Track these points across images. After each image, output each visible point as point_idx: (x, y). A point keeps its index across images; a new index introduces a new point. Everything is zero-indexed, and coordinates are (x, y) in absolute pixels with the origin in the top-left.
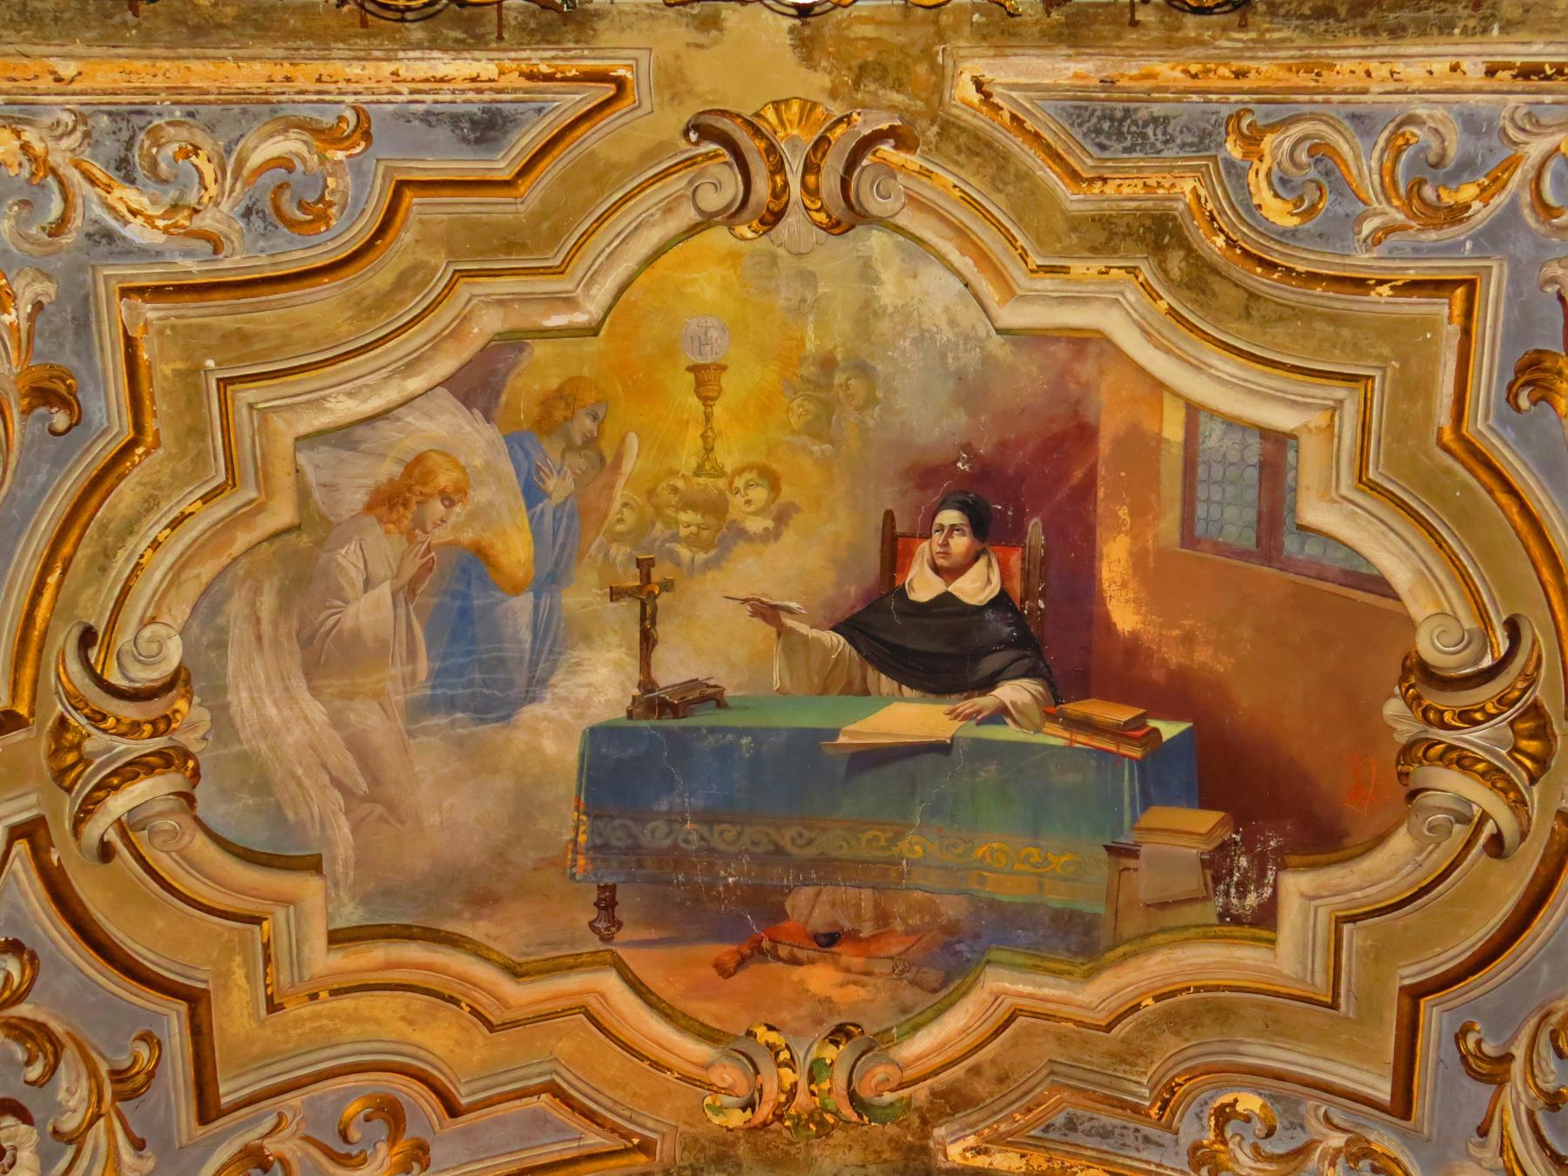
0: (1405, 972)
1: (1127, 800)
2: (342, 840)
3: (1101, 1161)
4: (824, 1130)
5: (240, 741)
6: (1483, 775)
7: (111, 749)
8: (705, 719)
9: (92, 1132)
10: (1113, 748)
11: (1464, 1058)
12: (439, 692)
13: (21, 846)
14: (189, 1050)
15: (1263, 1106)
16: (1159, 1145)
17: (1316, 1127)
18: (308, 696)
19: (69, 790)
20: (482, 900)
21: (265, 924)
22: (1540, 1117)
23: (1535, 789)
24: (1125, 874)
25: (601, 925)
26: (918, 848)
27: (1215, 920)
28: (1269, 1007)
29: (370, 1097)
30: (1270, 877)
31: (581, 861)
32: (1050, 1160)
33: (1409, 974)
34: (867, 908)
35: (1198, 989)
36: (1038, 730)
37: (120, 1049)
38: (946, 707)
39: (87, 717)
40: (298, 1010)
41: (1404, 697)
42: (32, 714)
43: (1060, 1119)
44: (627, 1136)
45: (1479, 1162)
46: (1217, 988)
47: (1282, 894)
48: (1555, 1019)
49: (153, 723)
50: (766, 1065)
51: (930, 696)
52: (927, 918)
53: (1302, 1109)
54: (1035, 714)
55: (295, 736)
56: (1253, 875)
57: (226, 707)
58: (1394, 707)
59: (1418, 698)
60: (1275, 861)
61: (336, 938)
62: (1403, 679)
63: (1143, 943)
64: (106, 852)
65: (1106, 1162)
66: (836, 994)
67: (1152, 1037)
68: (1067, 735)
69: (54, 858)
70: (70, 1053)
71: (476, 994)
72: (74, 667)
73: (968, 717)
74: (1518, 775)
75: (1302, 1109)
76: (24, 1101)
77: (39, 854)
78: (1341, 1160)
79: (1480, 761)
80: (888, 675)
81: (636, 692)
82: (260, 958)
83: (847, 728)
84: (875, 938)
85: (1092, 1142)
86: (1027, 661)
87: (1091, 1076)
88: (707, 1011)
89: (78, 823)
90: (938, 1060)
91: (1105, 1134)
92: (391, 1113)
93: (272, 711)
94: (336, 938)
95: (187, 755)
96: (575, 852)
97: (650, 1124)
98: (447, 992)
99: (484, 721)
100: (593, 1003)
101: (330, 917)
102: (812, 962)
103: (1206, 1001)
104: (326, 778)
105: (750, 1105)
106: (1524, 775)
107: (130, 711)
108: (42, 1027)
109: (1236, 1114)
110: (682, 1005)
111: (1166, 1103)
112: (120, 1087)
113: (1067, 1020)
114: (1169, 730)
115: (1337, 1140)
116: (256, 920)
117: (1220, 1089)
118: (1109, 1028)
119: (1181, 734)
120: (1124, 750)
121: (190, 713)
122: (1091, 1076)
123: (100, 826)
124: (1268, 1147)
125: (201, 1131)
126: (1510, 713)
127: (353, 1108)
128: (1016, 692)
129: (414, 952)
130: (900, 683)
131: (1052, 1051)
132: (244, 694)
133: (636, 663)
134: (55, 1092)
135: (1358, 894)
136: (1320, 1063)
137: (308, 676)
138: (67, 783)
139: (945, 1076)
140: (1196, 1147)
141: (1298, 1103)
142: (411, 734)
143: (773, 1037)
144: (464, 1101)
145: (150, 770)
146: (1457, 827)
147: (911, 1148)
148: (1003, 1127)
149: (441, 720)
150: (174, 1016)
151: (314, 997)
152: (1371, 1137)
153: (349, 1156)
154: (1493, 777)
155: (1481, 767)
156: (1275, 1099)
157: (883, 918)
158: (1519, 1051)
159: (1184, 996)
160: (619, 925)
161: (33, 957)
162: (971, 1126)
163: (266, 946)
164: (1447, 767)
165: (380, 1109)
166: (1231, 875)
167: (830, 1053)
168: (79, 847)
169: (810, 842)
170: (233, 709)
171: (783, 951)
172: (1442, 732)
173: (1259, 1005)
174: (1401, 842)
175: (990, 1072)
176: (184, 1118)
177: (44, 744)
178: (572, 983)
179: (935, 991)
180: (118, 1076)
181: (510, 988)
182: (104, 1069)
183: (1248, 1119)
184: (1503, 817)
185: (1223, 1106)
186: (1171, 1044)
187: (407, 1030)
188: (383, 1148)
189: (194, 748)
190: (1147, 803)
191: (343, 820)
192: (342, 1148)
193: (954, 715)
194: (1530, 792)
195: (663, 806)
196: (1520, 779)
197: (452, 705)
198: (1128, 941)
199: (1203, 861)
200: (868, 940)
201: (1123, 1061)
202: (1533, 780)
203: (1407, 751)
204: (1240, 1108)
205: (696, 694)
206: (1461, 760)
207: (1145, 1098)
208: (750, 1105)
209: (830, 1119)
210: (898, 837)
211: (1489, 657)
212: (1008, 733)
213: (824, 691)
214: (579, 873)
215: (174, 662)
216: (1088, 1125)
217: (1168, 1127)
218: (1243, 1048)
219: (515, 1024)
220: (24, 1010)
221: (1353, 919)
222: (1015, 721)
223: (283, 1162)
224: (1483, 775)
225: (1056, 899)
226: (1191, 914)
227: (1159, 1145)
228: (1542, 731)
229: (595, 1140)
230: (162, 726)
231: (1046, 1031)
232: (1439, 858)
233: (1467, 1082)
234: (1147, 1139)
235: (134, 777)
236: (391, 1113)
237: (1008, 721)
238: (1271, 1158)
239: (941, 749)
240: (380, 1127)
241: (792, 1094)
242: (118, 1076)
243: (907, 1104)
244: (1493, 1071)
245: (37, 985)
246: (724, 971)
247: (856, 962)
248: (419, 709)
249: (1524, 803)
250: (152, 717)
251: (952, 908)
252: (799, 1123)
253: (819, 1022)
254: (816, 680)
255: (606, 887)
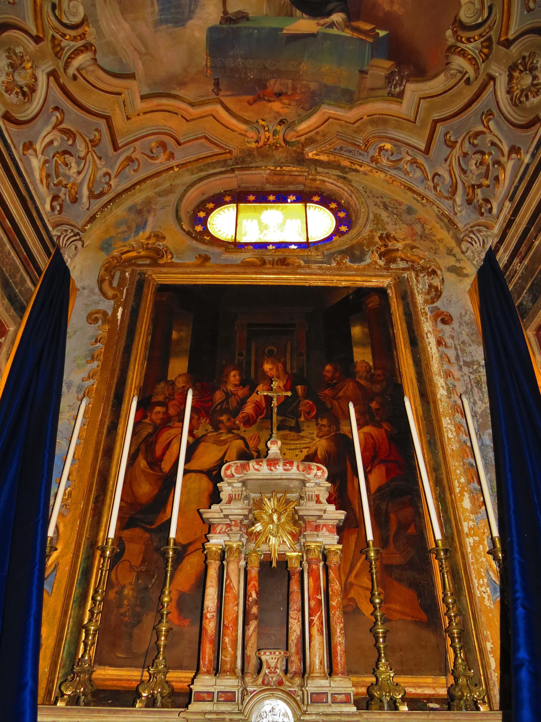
0: (435, 115)
1: (367, 56)
2: (140, 69)
3: (348, 159)
4: (277, 148)
5: (105, 38)
6: (469, 59)
7: (69, 45)
8: (243, 24)
9: (88, 157)
10: (364, 38)
11: (445, 141)
12: (162, 17)
13: (52, 78)
14: (108, 132)
15: (391, 148)
16: (364, 155)
17: (404, 154)
18: (123, 21)
19: (60, 59)
20: (182, 84)
21: (122, 95)
22: (461, 159)
23: (483, 65)
24: (363, 79)
25: (215, 91)
26: (305, 68)
27: (386, 95)
28: (397, 121)
29: (157, 142)
30: (404, 83)
31: (209, 71)
32: (335, 158)
33: (436, 116)
34: (290, 85)
35: (379, 114)
36: (343, 31)
37: (90, 133)
38: (317, 21)
39: (60, 35)
40: (134, 119)
41: (452, 30)
42: (44, 36)
43: (338, 147)
44: (225, 149)
45: (443, 167)
46: (384, 115)
47: (406, 89)
48: (471, 133)
49: (80, 36)
50: (261, 131)
51: (311, 17)
52: (307, 89)
53: (401, 149)
54: (343, 27)
55: (121, 35)
56: (399, 82)
57: (99, 27)
58: (449, 33)
59: (456, 32)
60: (406, 79)
61: (143, 98)
62: (453, 24)
63: (366, 100)
64: (75, 78)
65: (349, 159)
66: (281, 111)
67: (365, 127)
68: (351, 33)
69: (61, 82)
70: (78, 136)
71: (183, 112)
72: (52, 18)
73: (322, 25)
74: (479, 60)
75: (401, 149)
76: (69, 150)
77: (57, 80)
78: (409, 163)
79: (469, 55)
80: (299, 9)
81: (222, 15)
82: (123, 105)
83: (287, 28)
84: (292, 95)
85: (345, 153)
86: (341, 6)
87: (348, 136)
88: (246, 115)
89: (65, 69)
90: (308, 130)
91: (350, 152)
92: (163, 145)
93: (113, 27)
94: (143, 98)
95: (92, 45)
96: (207, 68)
97: (231, 146)
98: (175, 111)
99: (178, 27)
100: (215, 114)
101: (140, 92)
102: (274, 101)
103: (381, 118)
104: (133, 49)
105: (257, 142)
106: (481, 60)
107: (73, 33)
108: (69, 130)
109: (384, 149)
110: (238, 113)
111: (366, 145)
112: (93, 144)
113: (343, 121)
114: (382, 33)
115: (409, 158)
116: (120, 94)
117: (381, 142)
118: (354, 123)
119: (385, 35)
120: (368, 40)
121: (89, 30)
122: (348, 136)
123: (71, 71)
124: (391, 158)
125: (115, 153)
126: (482, 40)
127: (153, 144)
128: (338, 17)
129: (164, 101)
130: (302, 13)
131: (339, 129)
132: (104, 22)
133: (222, 5)
134: (76, 147)
135: (427, 92)
136: (409, 138)
137: (122, 14)
138: (59, 57)
139: (310, 134)
140: (373, 157)
141: (401, 147)
142: (156, 32)
143: (263, 123)
144: (182, 141)
145: (82, 52)
146: (458, 74)
147: (299, 153)
148: (323, 149)
149: (164, 27)
150: (102, 123)
151: (139, 115)
152: (418, 158)
153: (154, 157)
154: (472, 61)
155: (470, 57)
156: (395, 146)
157: (294, 89)
158: (460, 140)
159: (375, 116)
160: (220, 90)
161: (62, 111)
162: (315, 148)
163: (124, 102)
164: (460, 56)
165: (160, 144)
166: (393, 82)
167: (279, 128)
168: (67, 76)
169: (274, 65)
170: (102, 27)
171: (266, 98)
172: (461, 44)
173: (395, 120)
174: (442, 77)
175: (321, 133)
176: (110, 151)
177: (50, 45)
178: (208, 109)
179: (308, 110)
180: (91, 141)
181: (191, 110)
182: (87, 140)
183: (387, 151)
184: (471, 73)
185: (381, 147)
186: (370, 129)
187: (165, 122)
188: (162, 154)
189: (93, 42)
190: (373, 57)
191: (139, 62)
192: (151, 155)
193: (318, 24)
194: (481, 65)
195: (232, 53)
196: (480, 61)
197: (167, 21)
198: (362, 99)
199: (386, 77)
200: (289, 95)
201: (357, 133)
202: (483, 61)
203: (450, 47)
204: (385, 148)
205: (240, 15)
206: (463, 53)
207: (361, 143)
208: (257, 142)
209: (278, 145)
210: (300, 64)
211: (481, 18)
212: (334, 31)
213: (279, 15)
214: (208, 74)
215: (82, 15)
216: (345, 149)
217: (366, 151)
218: (388, 132)
219: (194, 119)
220: (63, 126)
221: (424, 98)
222: (336, 27)
223: (137, 159)
224: (469, 59)
225: (343, 85)
226: (380, 93)
227: (364, 155)
228: (489, 47)
229: (217, 150)
230: (83, 36)
231: (337, 123)
232: (452, 82)
233: (445, 147)
234: (360, 154)
235: (78, 55)
236: (163, 145)
237: (334, 27)
238: (392, 161)
239: (313, 35)
240: (161, 149)
241: (268, 139)
242: (91, 141)
243: (298, 142)
244: (452, 145)
245: (65, 118)
246: (250, 103)
247: (287, 101)
248: (158, 23)
249: (479, 69)
250: (79, 34)
251: (313, 86)
252: (270, 146)
253: (276, 119)
254: (277, 11)
255: (216, 79)
